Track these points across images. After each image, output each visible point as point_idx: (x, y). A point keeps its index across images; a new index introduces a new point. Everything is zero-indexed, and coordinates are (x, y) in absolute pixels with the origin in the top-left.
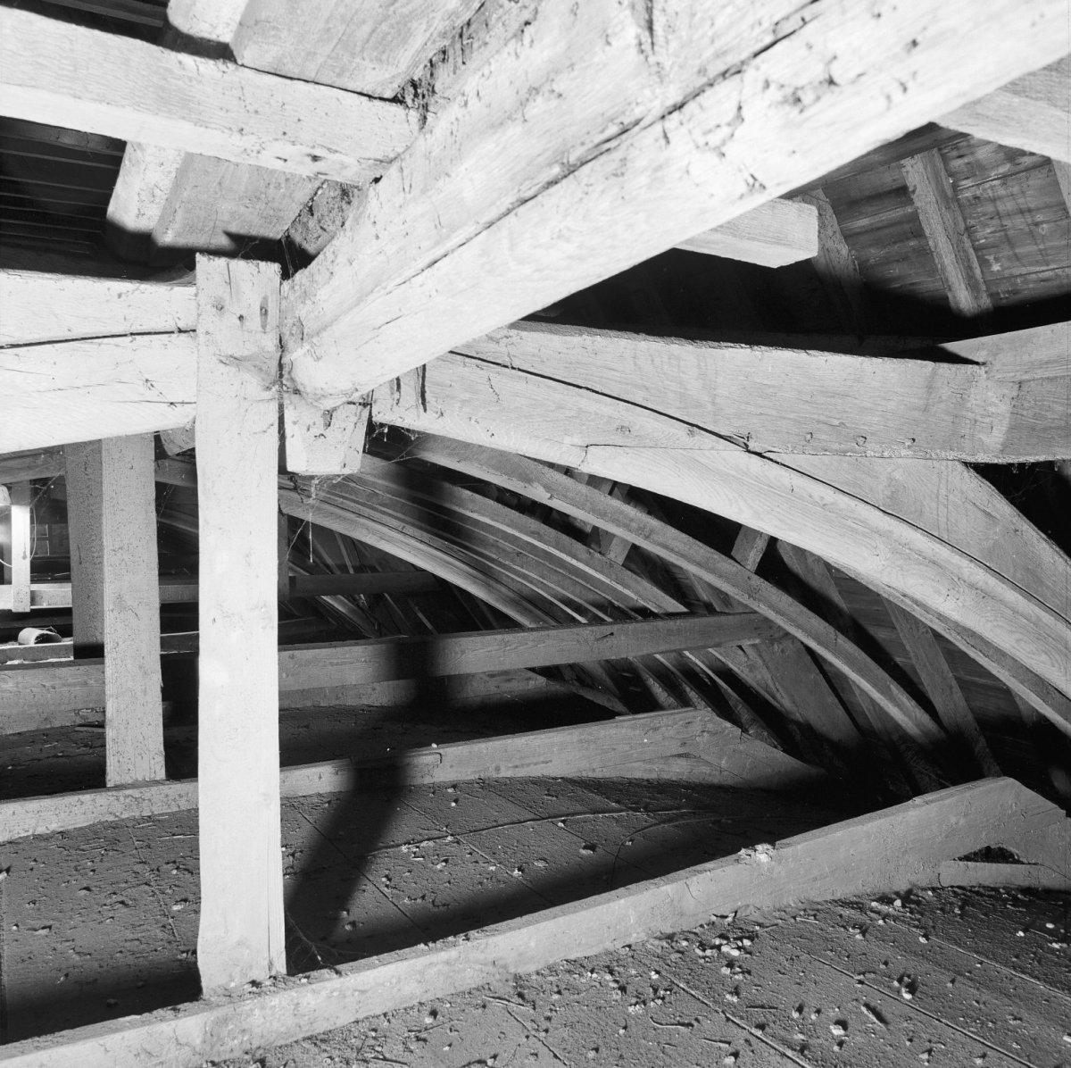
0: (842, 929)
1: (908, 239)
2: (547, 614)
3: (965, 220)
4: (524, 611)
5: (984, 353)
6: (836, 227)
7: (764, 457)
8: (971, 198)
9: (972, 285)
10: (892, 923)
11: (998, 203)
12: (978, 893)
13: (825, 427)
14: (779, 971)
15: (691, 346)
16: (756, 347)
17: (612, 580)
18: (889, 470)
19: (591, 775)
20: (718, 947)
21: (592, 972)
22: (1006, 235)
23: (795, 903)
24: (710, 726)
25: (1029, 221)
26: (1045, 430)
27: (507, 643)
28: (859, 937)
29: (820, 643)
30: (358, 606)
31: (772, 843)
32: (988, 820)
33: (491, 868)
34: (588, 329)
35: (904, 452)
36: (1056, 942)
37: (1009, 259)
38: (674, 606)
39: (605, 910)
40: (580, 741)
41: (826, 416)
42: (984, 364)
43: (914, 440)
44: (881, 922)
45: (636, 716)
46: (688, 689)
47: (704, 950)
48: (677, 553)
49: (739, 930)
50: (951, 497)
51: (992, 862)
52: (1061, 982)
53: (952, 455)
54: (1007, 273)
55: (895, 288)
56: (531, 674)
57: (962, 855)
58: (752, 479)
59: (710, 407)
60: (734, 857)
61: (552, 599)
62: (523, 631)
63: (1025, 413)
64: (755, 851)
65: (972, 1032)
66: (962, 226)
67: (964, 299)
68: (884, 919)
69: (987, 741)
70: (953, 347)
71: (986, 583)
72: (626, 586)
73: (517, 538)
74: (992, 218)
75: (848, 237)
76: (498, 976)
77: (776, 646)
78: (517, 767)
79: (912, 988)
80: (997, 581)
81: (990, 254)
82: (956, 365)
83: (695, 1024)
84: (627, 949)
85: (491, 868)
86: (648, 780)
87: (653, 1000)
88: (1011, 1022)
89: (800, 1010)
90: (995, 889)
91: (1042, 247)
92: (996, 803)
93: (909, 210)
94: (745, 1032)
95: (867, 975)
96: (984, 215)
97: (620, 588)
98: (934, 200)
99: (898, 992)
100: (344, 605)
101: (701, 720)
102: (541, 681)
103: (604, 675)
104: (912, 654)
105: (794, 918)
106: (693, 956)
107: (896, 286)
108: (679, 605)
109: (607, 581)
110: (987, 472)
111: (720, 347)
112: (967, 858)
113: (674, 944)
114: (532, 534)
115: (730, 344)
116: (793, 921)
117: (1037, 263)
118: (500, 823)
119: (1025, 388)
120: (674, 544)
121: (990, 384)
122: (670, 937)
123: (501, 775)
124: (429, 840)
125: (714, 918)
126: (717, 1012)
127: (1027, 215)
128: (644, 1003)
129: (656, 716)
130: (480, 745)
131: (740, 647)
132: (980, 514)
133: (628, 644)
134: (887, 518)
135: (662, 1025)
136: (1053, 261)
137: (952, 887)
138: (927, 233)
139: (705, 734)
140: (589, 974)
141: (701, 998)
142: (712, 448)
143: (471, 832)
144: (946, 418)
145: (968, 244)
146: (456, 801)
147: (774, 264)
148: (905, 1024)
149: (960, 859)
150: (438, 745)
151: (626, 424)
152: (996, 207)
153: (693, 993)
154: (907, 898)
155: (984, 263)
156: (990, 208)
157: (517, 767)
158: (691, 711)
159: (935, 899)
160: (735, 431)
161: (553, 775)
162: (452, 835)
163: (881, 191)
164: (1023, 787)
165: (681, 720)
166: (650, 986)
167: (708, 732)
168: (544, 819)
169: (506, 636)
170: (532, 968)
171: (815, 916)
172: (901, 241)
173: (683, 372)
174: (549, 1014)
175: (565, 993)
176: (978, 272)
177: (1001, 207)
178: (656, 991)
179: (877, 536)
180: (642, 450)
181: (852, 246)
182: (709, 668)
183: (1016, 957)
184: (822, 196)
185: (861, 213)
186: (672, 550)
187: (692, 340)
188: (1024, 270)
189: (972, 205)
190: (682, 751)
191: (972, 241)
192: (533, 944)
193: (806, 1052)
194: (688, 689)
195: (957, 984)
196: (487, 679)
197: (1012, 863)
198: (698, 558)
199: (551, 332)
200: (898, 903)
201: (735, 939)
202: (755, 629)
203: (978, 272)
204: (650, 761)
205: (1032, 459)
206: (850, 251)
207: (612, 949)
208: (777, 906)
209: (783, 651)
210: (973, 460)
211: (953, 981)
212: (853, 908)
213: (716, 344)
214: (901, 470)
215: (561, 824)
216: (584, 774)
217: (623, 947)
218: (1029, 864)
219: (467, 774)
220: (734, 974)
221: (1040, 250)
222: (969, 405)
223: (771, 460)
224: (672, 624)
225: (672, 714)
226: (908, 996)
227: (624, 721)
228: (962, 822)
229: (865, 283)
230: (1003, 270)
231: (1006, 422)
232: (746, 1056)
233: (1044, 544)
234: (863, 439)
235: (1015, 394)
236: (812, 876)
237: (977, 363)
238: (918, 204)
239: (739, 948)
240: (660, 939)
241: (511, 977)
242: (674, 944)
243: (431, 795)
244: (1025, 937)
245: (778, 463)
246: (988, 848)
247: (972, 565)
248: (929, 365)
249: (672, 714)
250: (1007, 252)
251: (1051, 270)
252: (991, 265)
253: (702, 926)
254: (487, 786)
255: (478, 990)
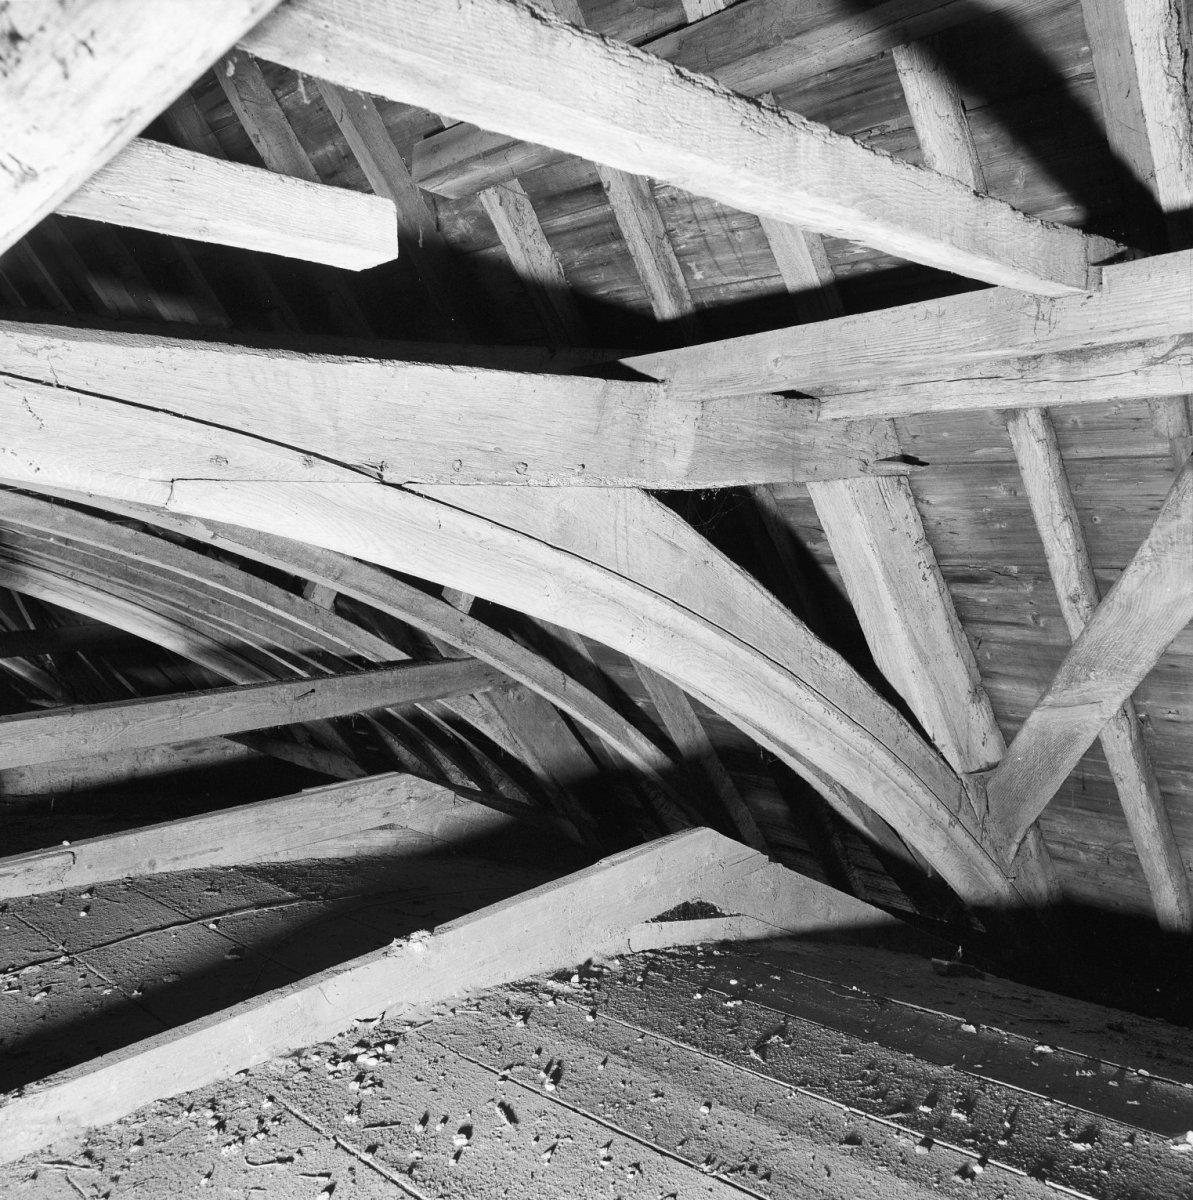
0: (504, 1018)
1: (610, 241)
2: (262, 668)
3: (664, 222)
4: (234, 667)
5: (663, 369)
6: (537, 225)
7: (406, 489)
8: (668, 199)
9: (675, 293)
10: (564, 1002)
11: (695, 206)
12: (672, 956)
13: (478, 454)
14: (416, 1078)
15: (304, 361)
16: (388, 362)
17: (318, 627)
18: (557, 500)
19: (274, 859)
20: (353, 1058)
21: (189, 1110)
22: (705, 241)
23: (459, 993)
24: (417, 791)
25: (725, 226)
26: (734, 453)
27: (182, 710)
28: (521, 1024)
29: (546, 689)
30: (43, 668)
31: (431, 929)
32: (682, 876)
33: (106, 992)
34: (164, 339)
35: (574, 480)
36: (731, 1000)
37: (710, 267)
38: (396, 654)
39: (213, 1033)
40: (259, 822)
41: (479, 440)
42: (663, 381)
43: (583, 466)
44: (551, 1004)
45: (328, 787)
46: (431, 747)
47: (336, 1064)
48: (374, 596)
49: (385, 1037)
50: (630, 527)
51: (689, 919)
52: (720, 1046)
53: (630, 482)
54: (709, 282)
55: (602, 295)
56: (228, 743)
57: (655, 916)
58: (390, 514)
59: (331, 433)
60: (384, 949)
61: (266, 652)
62: (234, 690)
63: (711, 435)
64: (408, 940)
65: (606, 1119)
66: (662, 231)
67: (666, 308)
68: (554, 1000)
69: (734, 781)
70: (633, 362)
71: (675, 621)
72: (335, 634)
73: (203, 584)
74: (690, 222)
75: (551, 236)
76: (64, 1135)
77: (511, 693)
78: (177, 859)
79: (556, 1077)
80: (686, 617)
81: (691, 261)
82: (630, 383)
83: (297, 1157)
84: (243, 1075)
85: (106, 992)
86: (343, 860)
87: (254, 1135)
88: (652, 1100)
89: (424, 1121)
90: (692, 948)
91: (740, 255)
92: (695, 858)
93: (596, 212)
94: (352, 1157)
95: (516, 1069)
96: (683, 218)
97: (329, 636)
98: (629, 199)
99: (542, 1084)
100: (25, 667)
101: (406, 786)
102: (240, 749)
103: (335, 734)
104: (652, 694)
105: (453, 1011)
106: (322, 1073)
107: (602, 292)
108: (400, 652)
109: (313, 629)
110: (673, 500)
111: (342, 362)
112: (661, 918)
113: (302, 1061)
114: (217, 577)
115: (355, 358)
116: (451, 1014)
117: (737, 272)
118: (136, 931)
119: (710, 407)
120: (370, 585)
121: (670, 403)
122: (298, 1054)
123: (157, 871)
124: (33, 964)
125: (357, 1024)
126: (328, 1139)
127: (723, 220)
128: (242, 1139)
129: (351, 785)
130: (126, 837)
131: (472, 696)
132: (666, 548)
133: (331, 701)
134: (556, 554)
135: (257, 1164)
136: (754, 272)
137: (644, 951)
138: (626, 235)
139: (411, 800)
140: (186, 1113)
141: (314, 1123)
142: (337, 480)
143: (94, 947)
144: (622, 441)
145: (669, 249)
146: (87, 909)
147: (357, 266)
148: (538, 1121)
149: (653, 921)
150: (70, 841)
151: (222, 454)
152: (692, 210)
153: (307, 1119)
154: (585, 970)
155: (686, 270)
156: (687, 211)
157: (177, 859)
158: (394, 776)
159: (621, 968)
160: (365, 460)
161: (224, 865)
162: (67, 954)
163: (579, 186)
164: (721, 836)
165: (381, 787)
166: (258, 1118)
167: (415, 798)
168: (194, 920)
169: (181, 701)
170: (114, 1117)
171: (477, 1005)
172: (604, 243)
173: (296, 392)
174: (119, 1173)
175: (148, 1142)
176: (681, 279)
177: (697, 211)
178: (261, 1121)
179: (547, 575)
180: (245, 483)
181: (555, 247)
182: (443, 719)
183: (682, 1024)
184: (519, 188)
185: (561, 211)
186: (368, 593)
187: (306, 353)
188: (725, 280)
189: (669, 206)
190: (385, 822)
191: (673, 246)
192: (114, 1088)
193: (415, 1172)
194: (431, 747)
195: (608, 1065)
196: (172, 751)
197: (712, 917)
198: (401, 601)
199: (113, 342)
200: (575, 978)
201: (377, 1045)
202: (486, 675)
203: (681, 279)
204: (346, 837)
205: (721, 485)
206: (553, 252)
207: (223, 1077)
208: (438, 999)
209: (519, 698)
210: (655, 487)
211: (604, 1063)
212: (524, 991)
213: (337, 357)
214: (572, 500)
215: (213, 926)
216: (265, 860)
217: (238, 1073)
218: (731, 915)
219: (112, 874)
220: (364, 1088)
221: (739, 259)
222: (647, 427)
223: (412, 492)
224: (388, 676)
225: (370, 781)
226: (550, 1088)
227: (313, 793)
228: (654, 880)
229: (572, 289)
230: (706, 278)
231: (690, 446)
232: (344, 1189)
233: (737, 576)
234: (524, 467)
235: (698, 414)
236: (480, 960)
237: (655, 381)
238: (613, 202)
239: (377, 1057)
240: (285, 1057)
241: (81, 1133)
242: (302, 1061)
243: (58, 905)
244: (701, 1000)
245: (421, 495)
246: (686, 904)
247: (657, 601)
248: (600, 382)
249: (370, 781)
250: (706, 260)
251: (751, 280)
252: (694, 274)
253: (341, 1035)
254: (137, 888)
255: (35, 1156)
